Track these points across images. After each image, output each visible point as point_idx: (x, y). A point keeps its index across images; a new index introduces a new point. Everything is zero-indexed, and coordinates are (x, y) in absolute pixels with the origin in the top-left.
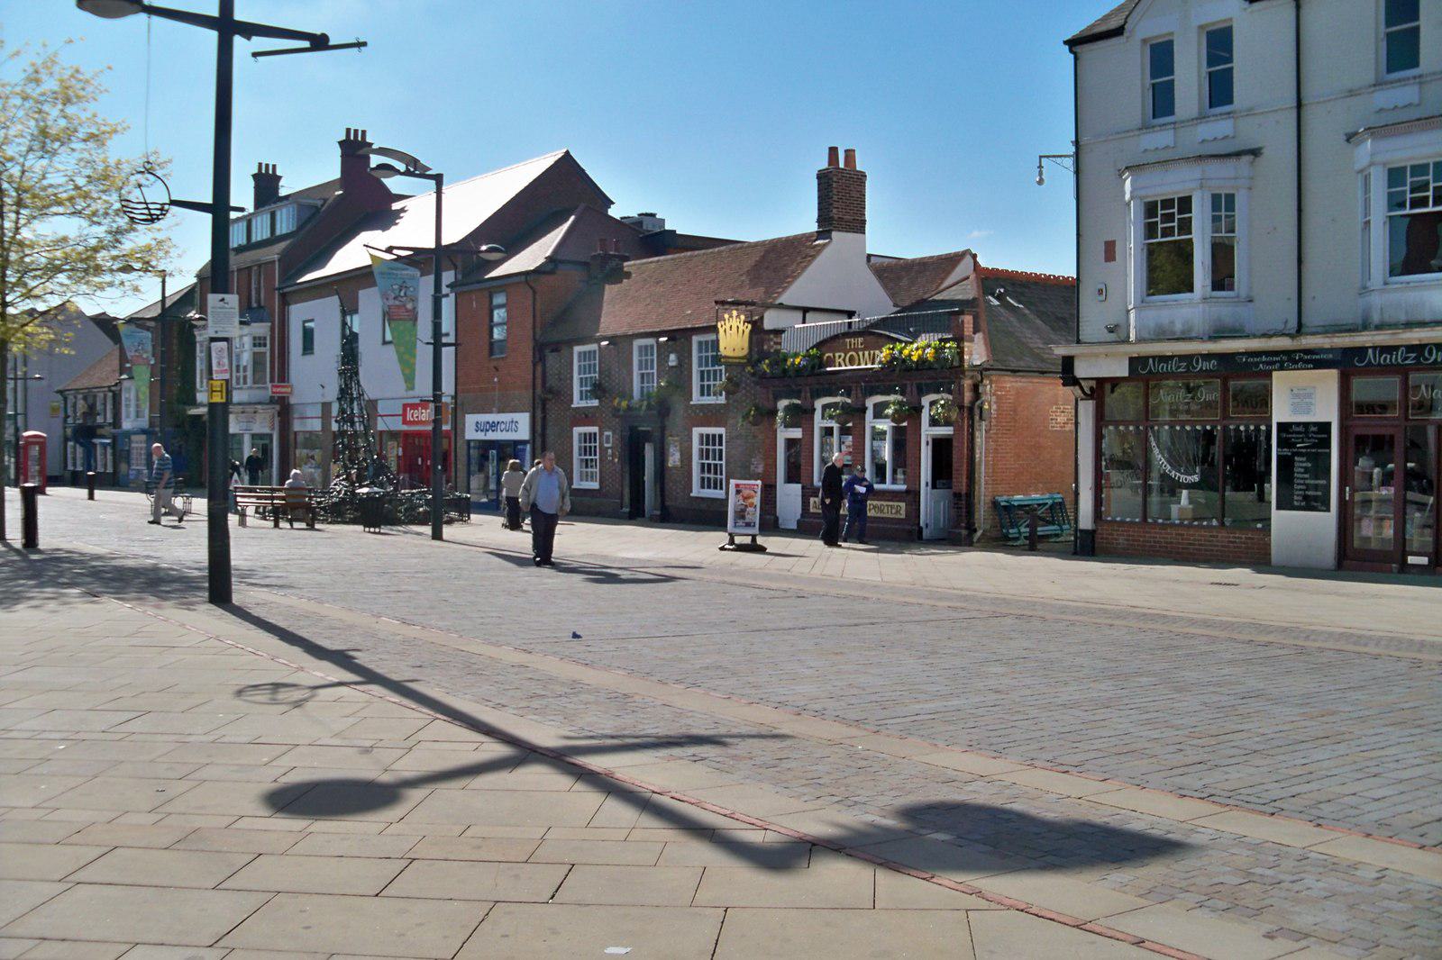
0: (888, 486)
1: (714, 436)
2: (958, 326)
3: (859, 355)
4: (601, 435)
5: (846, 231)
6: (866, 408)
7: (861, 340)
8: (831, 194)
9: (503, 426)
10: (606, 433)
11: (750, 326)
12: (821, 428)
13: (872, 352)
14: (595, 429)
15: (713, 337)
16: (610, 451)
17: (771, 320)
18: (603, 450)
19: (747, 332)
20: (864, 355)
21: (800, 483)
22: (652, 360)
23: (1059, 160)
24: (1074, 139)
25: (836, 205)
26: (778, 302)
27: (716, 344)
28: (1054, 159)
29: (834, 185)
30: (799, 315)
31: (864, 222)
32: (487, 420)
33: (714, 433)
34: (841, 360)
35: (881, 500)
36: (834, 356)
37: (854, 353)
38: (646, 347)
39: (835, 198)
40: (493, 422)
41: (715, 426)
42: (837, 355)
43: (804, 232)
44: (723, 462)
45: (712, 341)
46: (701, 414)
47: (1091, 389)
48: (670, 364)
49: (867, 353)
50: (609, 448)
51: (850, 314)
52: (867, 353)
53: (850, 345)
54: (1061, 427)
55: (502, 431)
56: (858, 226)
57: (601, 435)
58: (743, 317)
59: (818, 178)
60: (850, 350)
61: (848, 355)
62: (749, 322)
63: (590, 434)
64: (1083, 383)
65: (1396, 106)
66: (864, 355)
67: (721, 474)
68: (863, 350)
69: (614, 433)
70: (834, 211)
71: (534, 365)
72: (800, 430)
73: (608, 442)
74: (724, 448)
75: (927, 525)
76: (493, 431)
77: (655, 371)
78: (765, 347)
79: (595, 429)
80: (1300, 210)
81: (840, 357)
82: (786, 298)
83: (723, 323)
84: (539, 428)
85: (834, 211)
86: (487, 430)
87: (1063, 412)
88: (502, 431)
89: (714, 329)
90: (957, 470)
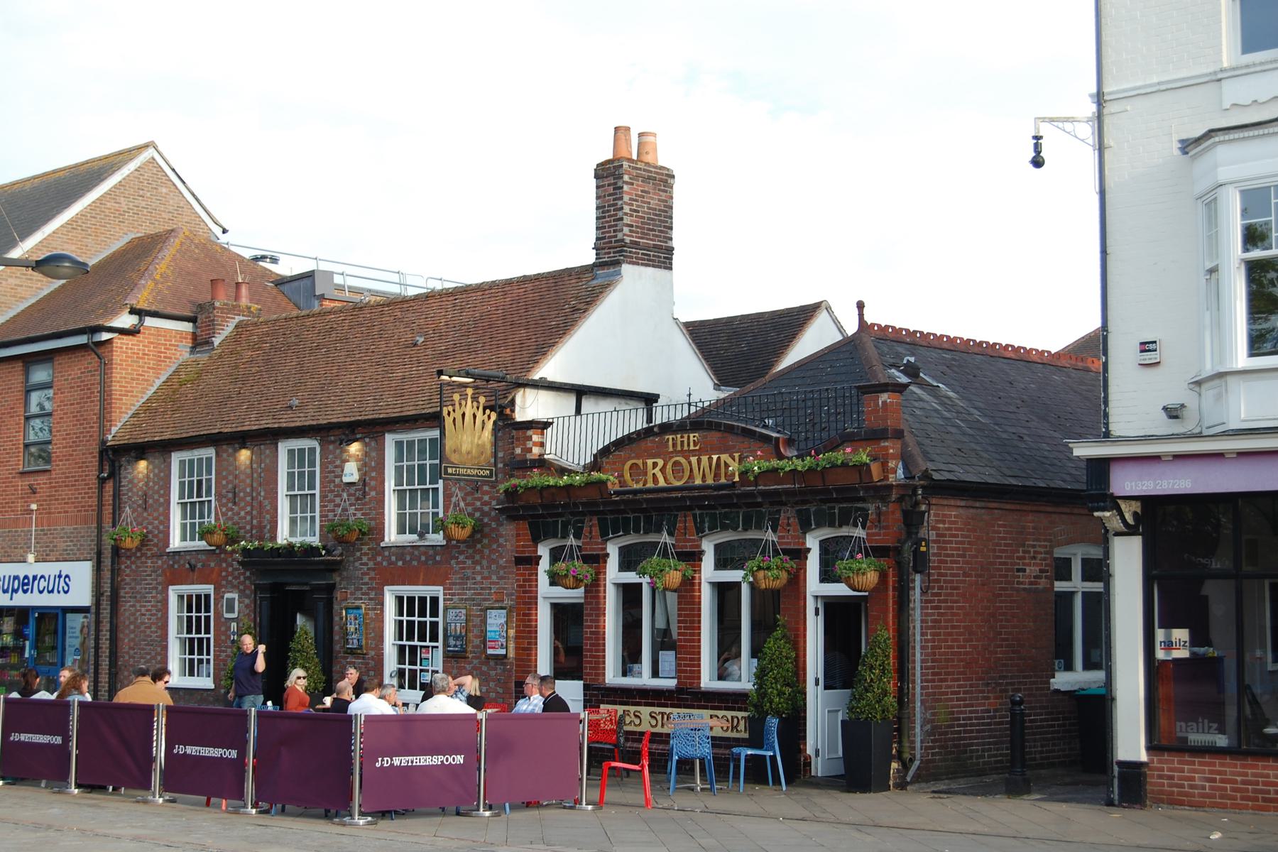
0: (644, 678)
1: (423, 600)
2: (876, 411)
3: (690, 463)
4: (219, 598)
5: (654, 266)
6: (702, 553)
7: (694, 436)
8: (620, 203)
9: (43, 584)
10: (227, 596)
11: (494, 416)
12: (617, 585)
13: (715, 457)
14: (209, 589)
15: (435, 433)
16: (234, 625)
17: (530, 406)
18: (223, 624)
19: (490, 425)
20: (699, 461)
21: (580, 678)
22: (312, 474)
23: (1068, 126)
24: (1094, 90)
25: (627, 220)
26: (536, 377)
27: (437, 447)
28: (1060, 125)
29: (626, 188)
30: (571, 401)
31: (670, 250)
32: (13, 574)
33: (198, 592)
34: (657, 471)
35: (733, 709)
36: (645, 464)
37: (683, 460)
38: (301, 451)
39: (627, 209)
40: (26, 577)
41: (426, 583)
42: (650, 462)
43: (469, 283)
44: (211, 636)
45: (433, 441)
46: (400, 563)
47: (1135, 514)
48: (346, 479)
49: (705, 459)
50: (233, 620)
51: (649, 400)
52: (705, 459)
53: (674, 445)
54: (1031, 583)
55: (41, 592)
56: (661, 257)
57: (219, 598)
58: (482, 400)
59: (597, 176)
60: (676, 452)
61: (670, 464)
62: (492, 409)
63: (199, 597)
64: (1123, 506)
65: (1256, 101)
66: (699, 461)
67: (208, 654)
68: (699, 453)
69: (242, 594)
70: (626, 230)
71: (102, 481)
72: (1056, 589)
73: (231, 609)
74: (440, 619)
75: (817, 752)
76: (25, 592)
77: (317, 492)
78: (518, 451)
79: (209, 589)
80: (1104, 252)
81: (655, 465)
82: (536, 375)
83: (450, 408)
84: (107, 588)
85: (626, 230)
86: (16, 591)
87: (1034, 558)
88: (41, 592)
89: (435, 420)
90: (72, 628)
